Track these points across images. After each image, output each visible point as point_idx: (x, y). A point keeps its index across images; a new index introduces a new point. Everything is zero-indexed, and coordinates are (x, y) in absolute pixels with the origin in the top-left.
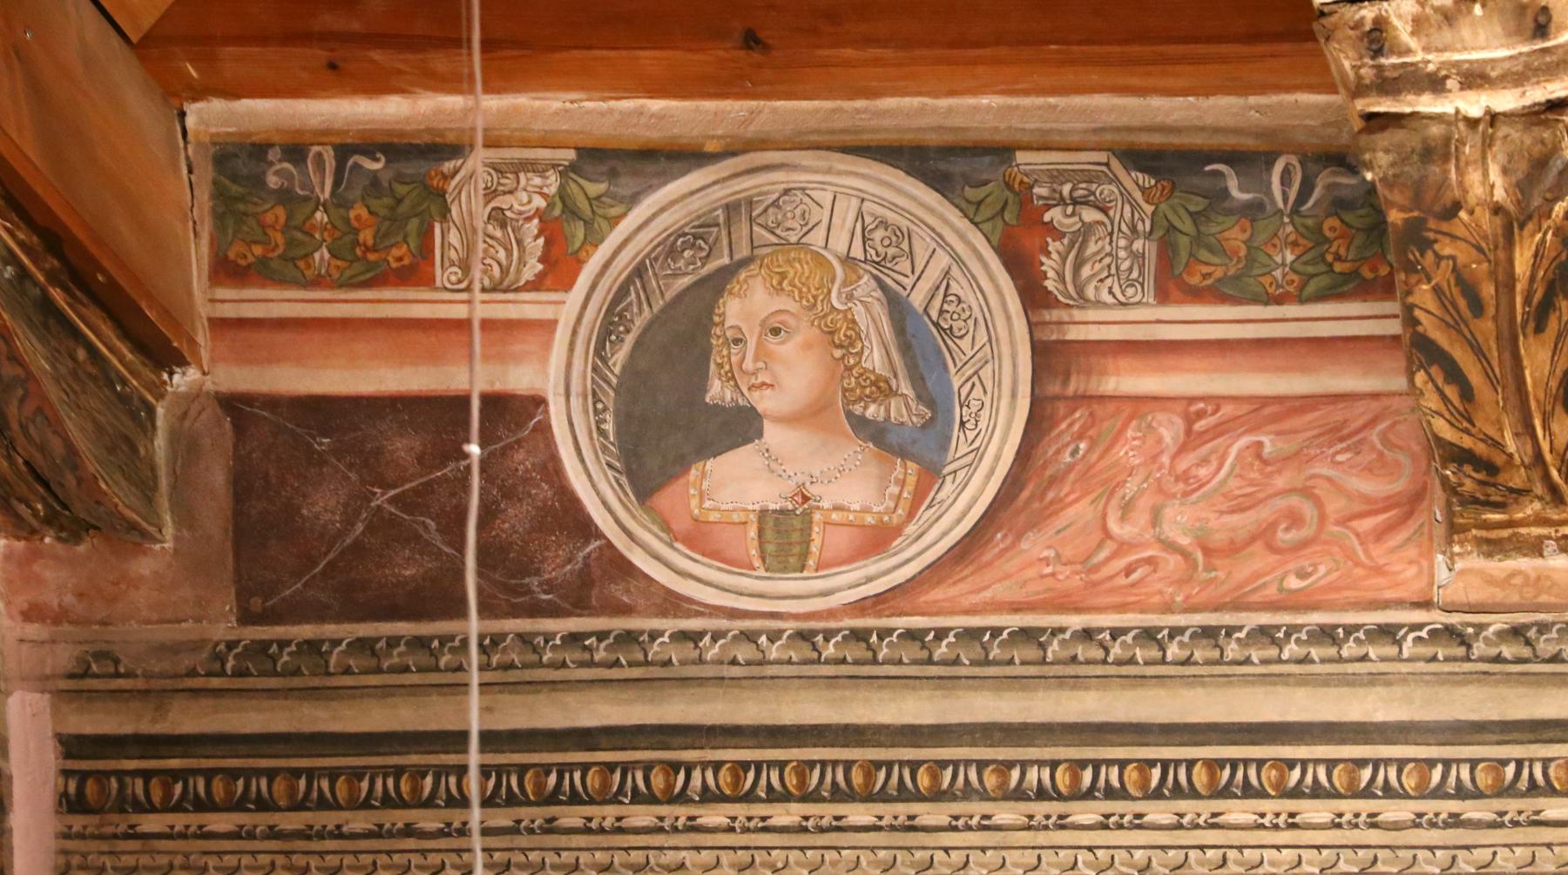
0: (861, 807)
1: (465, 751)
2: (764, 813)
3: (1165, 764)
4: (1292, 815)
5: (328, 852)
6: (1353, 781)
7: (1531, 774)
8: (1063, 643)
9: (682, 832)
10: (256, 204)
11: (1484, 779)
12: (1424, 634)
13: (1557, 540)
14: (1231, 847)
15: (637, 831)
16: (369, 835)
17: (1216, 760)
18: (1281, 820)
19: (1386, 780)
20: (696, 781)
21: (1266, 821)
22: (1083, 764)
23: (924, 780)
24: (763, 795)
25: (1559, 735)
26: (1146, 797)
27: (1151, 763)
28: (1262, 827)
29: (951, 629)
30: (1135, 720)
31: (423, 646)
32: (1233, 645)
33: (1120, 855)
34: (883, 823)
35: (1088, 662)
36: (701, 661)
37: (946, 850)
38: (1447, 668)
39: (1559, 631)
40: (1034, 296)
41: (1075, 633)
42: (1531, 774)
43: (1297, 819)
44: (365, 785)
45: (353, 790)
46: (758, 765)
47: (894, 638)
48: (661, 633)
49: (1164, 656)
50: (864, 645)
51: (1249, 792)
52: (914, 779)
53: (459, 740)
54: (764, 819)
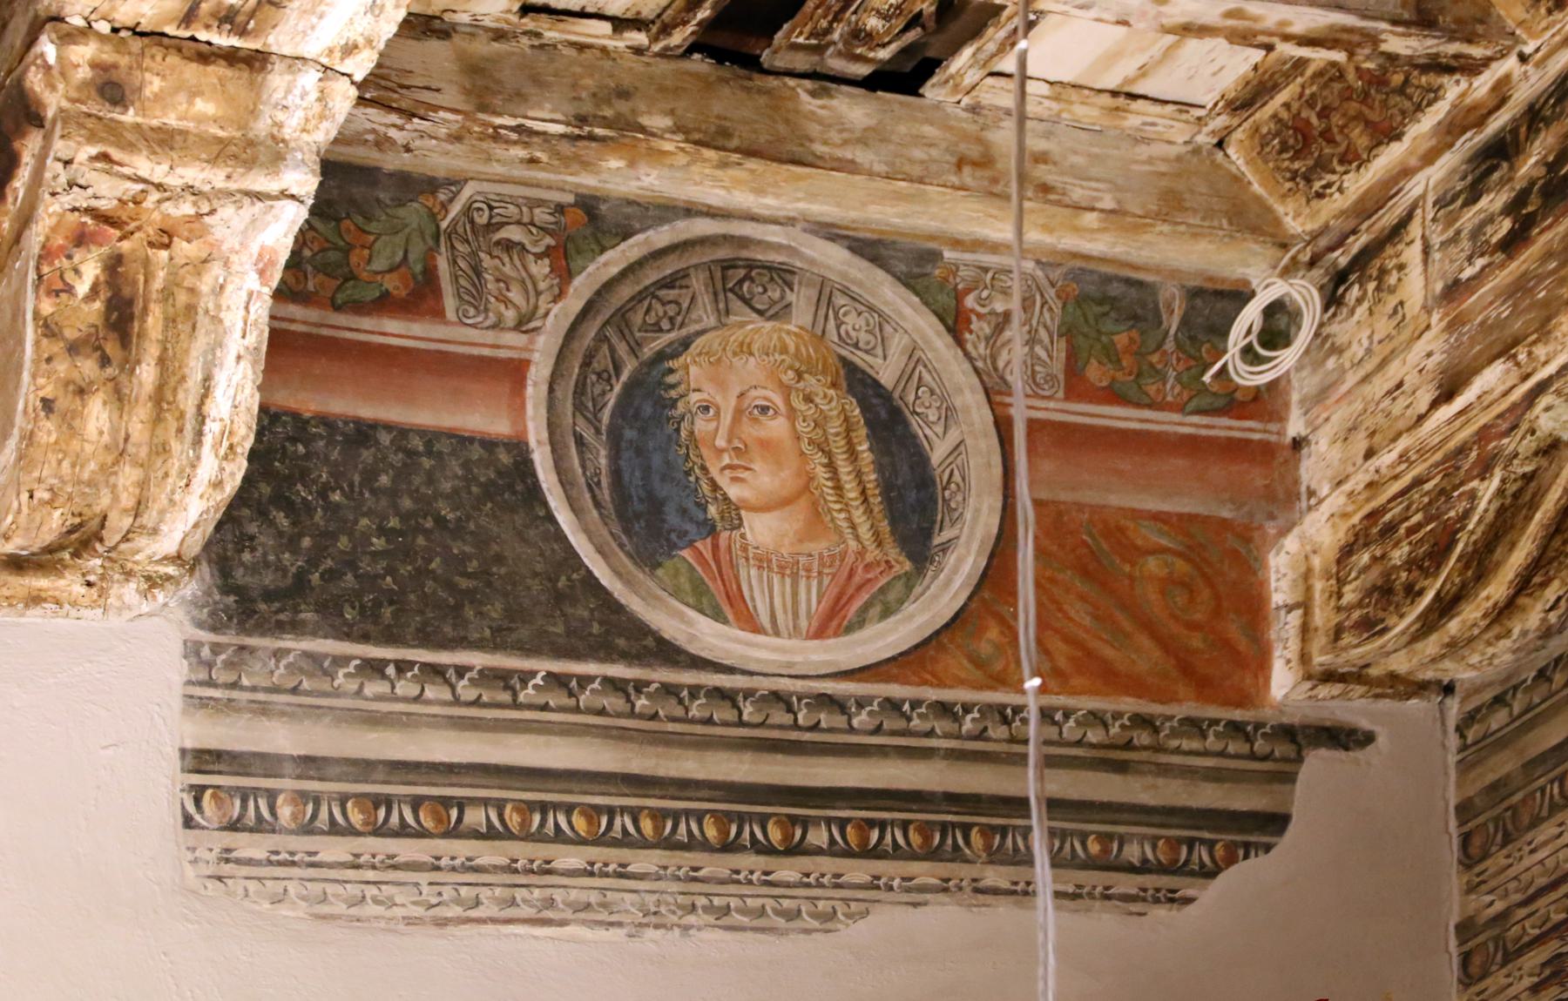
1: (1028, 817)
2: (1173, 886)
4: (838, 876)
15: (331, 866)
16: (496, 869)
21: (741, 877)
22: (871, 823)
35: (831, 730)
41: (930, 706)
47: (876, 708)
48: (533, 674)
49: (796, 720)
53: (1019, 805)
54: (310, 854)
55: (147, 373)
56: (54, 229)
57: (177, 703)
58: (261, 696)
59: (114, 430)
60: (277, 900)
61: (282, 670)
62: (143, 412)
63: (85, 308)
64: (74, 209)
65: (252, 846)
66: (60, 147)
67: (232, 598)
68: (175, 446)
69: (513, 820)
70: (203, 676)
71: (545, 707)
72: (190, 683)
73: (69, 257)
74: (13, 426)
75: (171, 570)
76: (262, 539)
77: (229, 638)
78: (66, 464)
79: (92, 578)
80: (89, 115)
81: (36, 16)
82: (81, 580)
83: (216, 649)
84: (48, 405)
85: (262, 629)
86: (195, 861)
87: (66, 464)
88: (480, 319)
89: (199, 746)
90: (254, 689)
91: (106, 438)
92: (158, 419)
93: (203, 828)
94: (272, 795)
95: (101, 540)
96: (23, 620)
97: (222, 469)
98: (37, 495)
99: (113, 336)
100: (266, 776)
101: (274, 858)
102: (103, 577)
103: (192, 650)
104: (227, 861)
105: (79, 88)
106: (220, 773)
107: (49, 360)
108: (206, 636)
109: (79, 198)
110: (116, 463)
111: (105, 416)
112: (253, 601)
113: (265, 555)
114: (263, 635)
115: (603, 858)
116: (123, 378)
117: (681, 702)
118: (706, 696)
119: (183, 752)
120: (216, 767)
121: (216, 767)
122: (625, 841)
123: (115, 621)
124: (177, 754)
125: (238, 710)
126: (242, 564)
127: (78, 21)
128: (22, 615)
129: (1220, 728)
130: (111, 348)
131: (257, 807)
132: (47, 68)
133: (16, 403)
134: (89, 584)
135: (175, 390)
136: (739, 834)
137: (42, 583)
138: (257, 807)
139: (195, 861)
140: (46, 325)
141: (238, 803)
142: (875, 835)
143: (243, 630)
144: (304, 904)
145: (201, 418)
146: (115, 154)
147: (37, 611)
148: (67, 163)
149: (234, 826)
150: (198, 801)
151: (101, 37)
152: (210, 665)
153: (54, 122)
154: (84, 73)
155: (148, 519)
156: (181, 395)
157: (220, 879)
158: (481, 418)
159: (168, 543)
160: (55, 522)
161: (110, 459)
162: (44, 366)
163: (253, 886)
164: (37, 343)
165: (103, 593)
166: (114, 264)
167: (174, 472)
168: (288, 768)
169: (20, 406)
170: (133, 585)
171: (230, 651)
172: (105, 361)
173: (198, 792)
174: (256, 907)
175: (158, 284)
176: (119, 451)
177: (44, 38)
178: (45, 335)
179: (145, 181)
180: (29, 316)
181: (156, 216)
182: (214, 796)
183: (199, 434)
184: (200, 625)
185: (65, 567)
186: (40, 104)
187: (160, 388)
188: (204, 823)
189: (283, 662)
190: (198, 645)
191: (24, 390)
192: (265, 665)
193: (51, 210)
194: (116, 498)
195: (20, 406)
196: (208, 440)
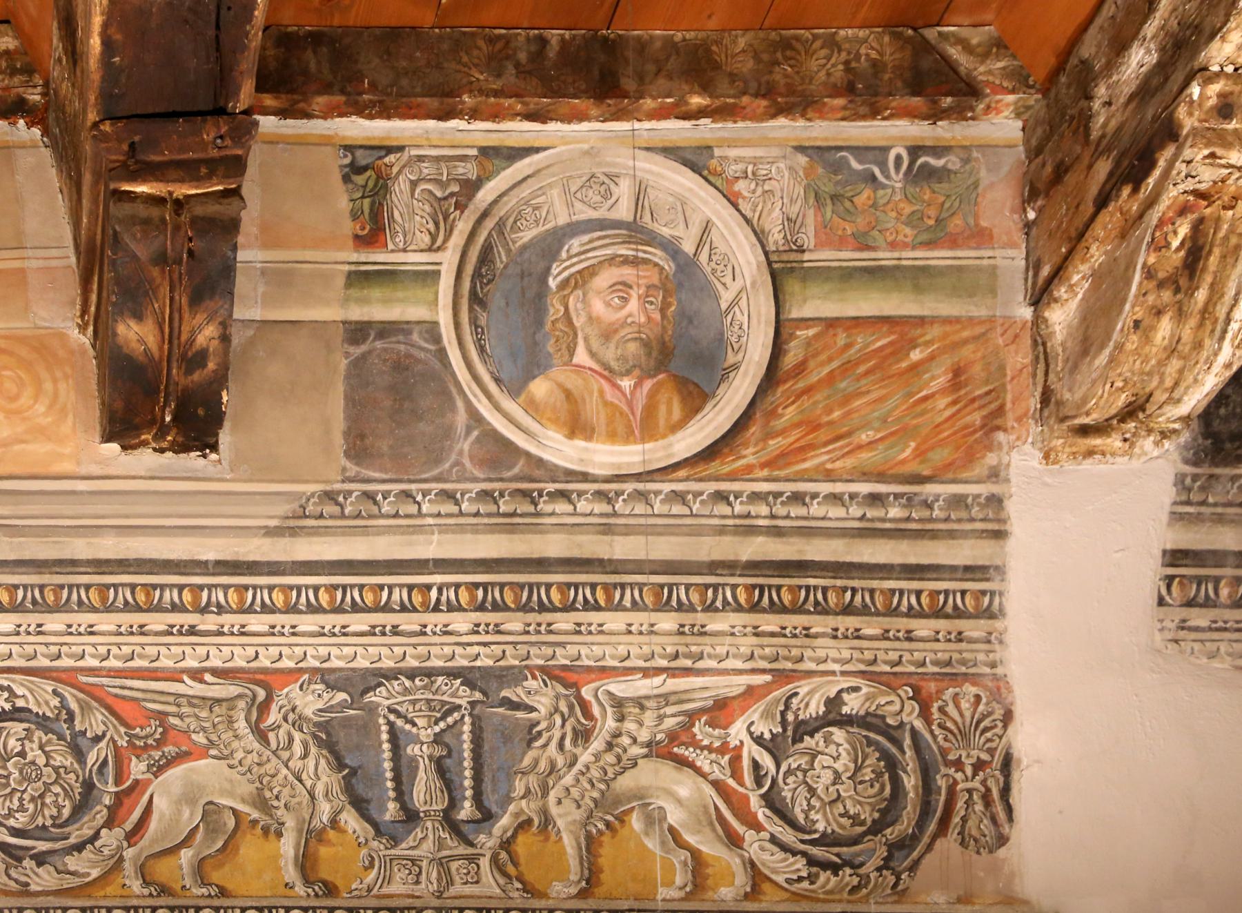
0: (923, 622)
3: (344, 588)
7: (262, 599)
8: (702, 502)
10: (134, 236)
11: (369, 598)
15: (303, 634)
18: (235, 630)
23: (50, 598)
26: (705, 610)
27: (246, 588)
30: (535, 556)
32: (698, 505)
36: (420, 514)
38: (486, 520)
41: (826, 497)
43: (43, 629)
44: (525, 594)
45: (197, 599)
47: (432, 496)
48: (350, 493)
51: (267, 609)
52: (825, 599)
55: (1201, 295)
56: (1169, 208)
57: (1165, 518)
58: (1219, 510)
59: (1172, 335)
60: (1212, 656)
61: (1235, 490)
62: (1193, 322)
63: (1174, 256)
64: (1185, 192)
65: (1200, 618)
66: (1187, 153)
67: (1209, 441)
68: (1207, 342)
69: (324, 598)
70: (1184, 498)
72: (1175, 503)
73: (1173, 224)
74: (1110, 340)
75: (1177, 426)
76: (1234, 397)
77: (1204, 470)
78: (1138, 362)
79: (1128, 436)
80: (1208, 129)
81: (1192, 69)
82: (1120, 437)
83: (1195, 478)
84: (1137, 324)
85: (1226, 462)
86: (1161, 630)
87: (1138, 362)
89: (1175, 547)
90: (1215, 505)
91: (1166, 342)
92: (1201, 325)
93: (1170, 605)
94: (1217, 581)
95: (1144, 410)
96: (1080, 467)
97: (1234, 354)
98: (1116, 385)
99: (1187, 272)
100: (1216, 566)
101: (1214, 625)
102: (1134, 435)
103: (1180, 480)
104: (1183, 628)
105: (1207, 112)
106: (1186, 566)
107: (1144, 295)
108: (1189, 469)
109: (1190, 185)
110: (1168, 358)
111: (1169, 327)
112: (1223, 442)
113: (1234, 408)
114: (1226, 466)
115: (699, 623)
116: (1185, 301)
119: (1165, 552)
120: (1184, 562)
121: (1184, 562)
122: (496, 607)
123: (1136, 464)
124: (1160, 554)
125: (1203, 521)
126: (1218, 416)
127: (1216, 68)
128: (1080, 464)
130: (1183, 282)
131: (1207, 589)
132: (1192, 102)
133: (1116, 325)
134: (1125, 440)
135: (1215, 304)
137: (1097, 441)
138: (1207, 589)
139: (1161, 630)
140: (1149, 272)
141: (1194, 587)
143: (1215, 464)
144: (1229, 659)
145: (1228, 320)
146: (1219, 152)
147: (1090, 461)
148: (1189, 162)
149: (1190, 603)
150: (1169, 587)
151: (1227, 76)
152: (1189, 490)
153: (1187, 136)
154: (1213, 101)
155: (1176, 395)
156: (1218, 307)
157: (1176, 641)
158: (414, 312)
159: (1184, 409)
160: (1122, 400)
161: (1164, 356)
162: (1141, 298)
163: (1197, 646)
164: (1141, 283)
165: (1132, 445)
166: (1197, 227)
167: (1202, 361)
168: (1231, 560)
169: (1119, 327)
170: (1152, 438)
171: (1203, 479)
172: (1177, 290)
173: (1169, 580)
174: (1198, 662)
175: (1221, 234)
176: (1172, 350)
177: (1195, 83)
178: (1146, 278)
179: (1232, 166)
180: (1139, 267)
181: (1233, 188)
182: (1180, 583)
183: (1225, 331)
184: (1186, 461)
185: (1113, 429)
186: (1181, 126)
187: (1207, 304)
188: (1170, 602)
189: (1237, 484)
190: (1184, 476)
191: (1124, 316)
192: (1224, 487)
193: (1172, 194)
194: (1162, 381)
195: (1119, 327)
196: (1229, 335)
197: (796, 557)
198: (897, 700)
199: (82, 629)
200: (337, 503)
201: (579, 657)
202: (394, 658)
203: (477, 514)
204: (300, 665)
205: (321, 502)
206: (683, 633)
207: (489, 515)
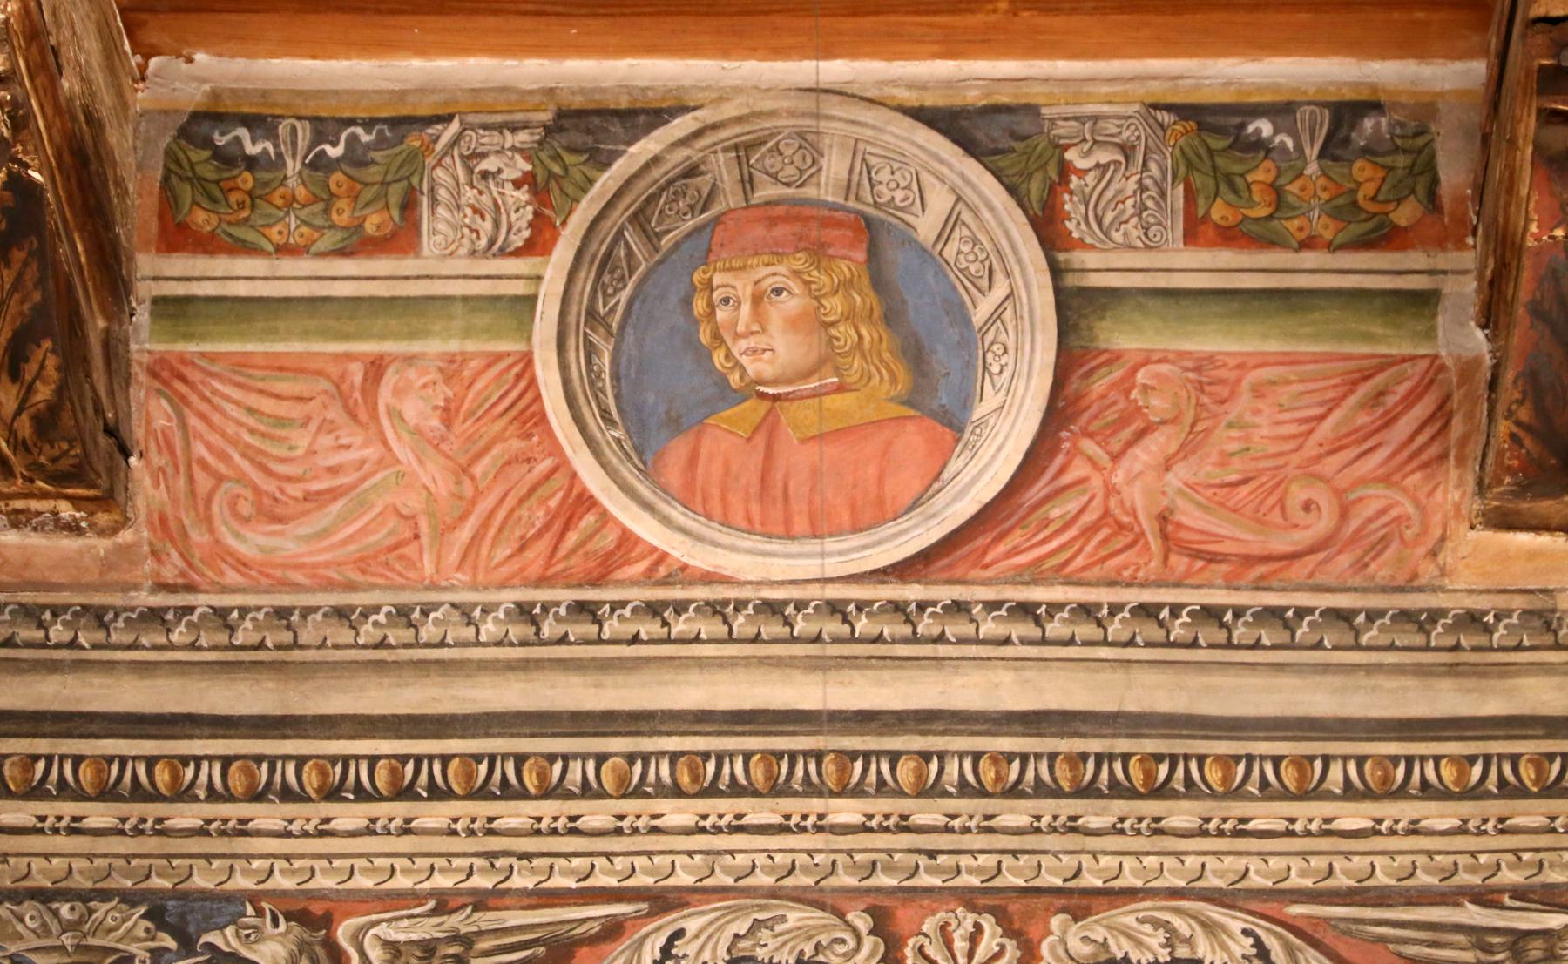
2: (78, 813)
5: (1187, 853)
6: (1386, 779)
9: (313, 836)
12: (938, 609)
13: (8, 514)
14: (678, 853)
17: (104, 757)
19: (1037, 776)
20: (952, 769)
24: (1256, 791)
25: (14, 728)
28: (538, 832)
29: (693, 601)
31: (774, 613)
33: (842, 859)
34: (708, 823)
37: (1094, 854)
39: (11, 613)
40: (1048, 228)
42: (504, 774)
46: (867, 755)
47: (1387, 620)
50: (967, 617)
71: (635, 640)
88: (245, 214)
117: (1161, 624)
118: (1189, 614)
129: (1515, 620)
136: (791, 773)
142: (1163, 770)
197: (277, 711)
198: (848, 936)
199: (1314, 827)
200: (1222, 625)
201: (1331, 872)
202: (615, 873)
203: (817, 639)
204: (1366, 884)
205: (1523, 626)
206: (454, 833)
207: (837, 640)
